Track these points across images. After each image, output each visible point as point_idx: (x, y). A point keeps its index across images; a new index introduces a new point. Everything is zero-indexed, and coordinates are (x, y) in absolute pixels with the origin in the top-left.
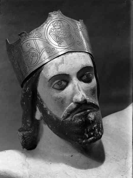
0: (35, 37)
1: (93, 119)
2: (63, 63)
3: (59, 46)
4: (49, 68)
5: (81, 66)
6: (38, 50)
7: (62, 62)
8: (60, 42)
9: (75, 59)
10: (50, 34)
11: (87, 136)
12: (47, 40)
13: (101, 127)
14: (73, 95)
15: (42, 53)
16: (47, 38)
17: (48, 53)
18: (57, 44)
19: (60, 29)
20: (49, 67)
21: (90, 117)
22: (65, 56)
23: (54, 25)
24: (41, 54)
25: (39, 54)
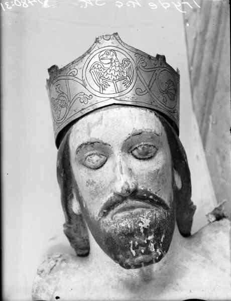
1: (147, 226)
2: (101, 124)
3: (101, 92)
6: (69, 96)
7: (100, 121)
8: (103, 87)
10: (91, 71)
11: (134, 252)
13: (162, 241)
14: (113, 182)
18: (98, 89)
23: (101, 57)
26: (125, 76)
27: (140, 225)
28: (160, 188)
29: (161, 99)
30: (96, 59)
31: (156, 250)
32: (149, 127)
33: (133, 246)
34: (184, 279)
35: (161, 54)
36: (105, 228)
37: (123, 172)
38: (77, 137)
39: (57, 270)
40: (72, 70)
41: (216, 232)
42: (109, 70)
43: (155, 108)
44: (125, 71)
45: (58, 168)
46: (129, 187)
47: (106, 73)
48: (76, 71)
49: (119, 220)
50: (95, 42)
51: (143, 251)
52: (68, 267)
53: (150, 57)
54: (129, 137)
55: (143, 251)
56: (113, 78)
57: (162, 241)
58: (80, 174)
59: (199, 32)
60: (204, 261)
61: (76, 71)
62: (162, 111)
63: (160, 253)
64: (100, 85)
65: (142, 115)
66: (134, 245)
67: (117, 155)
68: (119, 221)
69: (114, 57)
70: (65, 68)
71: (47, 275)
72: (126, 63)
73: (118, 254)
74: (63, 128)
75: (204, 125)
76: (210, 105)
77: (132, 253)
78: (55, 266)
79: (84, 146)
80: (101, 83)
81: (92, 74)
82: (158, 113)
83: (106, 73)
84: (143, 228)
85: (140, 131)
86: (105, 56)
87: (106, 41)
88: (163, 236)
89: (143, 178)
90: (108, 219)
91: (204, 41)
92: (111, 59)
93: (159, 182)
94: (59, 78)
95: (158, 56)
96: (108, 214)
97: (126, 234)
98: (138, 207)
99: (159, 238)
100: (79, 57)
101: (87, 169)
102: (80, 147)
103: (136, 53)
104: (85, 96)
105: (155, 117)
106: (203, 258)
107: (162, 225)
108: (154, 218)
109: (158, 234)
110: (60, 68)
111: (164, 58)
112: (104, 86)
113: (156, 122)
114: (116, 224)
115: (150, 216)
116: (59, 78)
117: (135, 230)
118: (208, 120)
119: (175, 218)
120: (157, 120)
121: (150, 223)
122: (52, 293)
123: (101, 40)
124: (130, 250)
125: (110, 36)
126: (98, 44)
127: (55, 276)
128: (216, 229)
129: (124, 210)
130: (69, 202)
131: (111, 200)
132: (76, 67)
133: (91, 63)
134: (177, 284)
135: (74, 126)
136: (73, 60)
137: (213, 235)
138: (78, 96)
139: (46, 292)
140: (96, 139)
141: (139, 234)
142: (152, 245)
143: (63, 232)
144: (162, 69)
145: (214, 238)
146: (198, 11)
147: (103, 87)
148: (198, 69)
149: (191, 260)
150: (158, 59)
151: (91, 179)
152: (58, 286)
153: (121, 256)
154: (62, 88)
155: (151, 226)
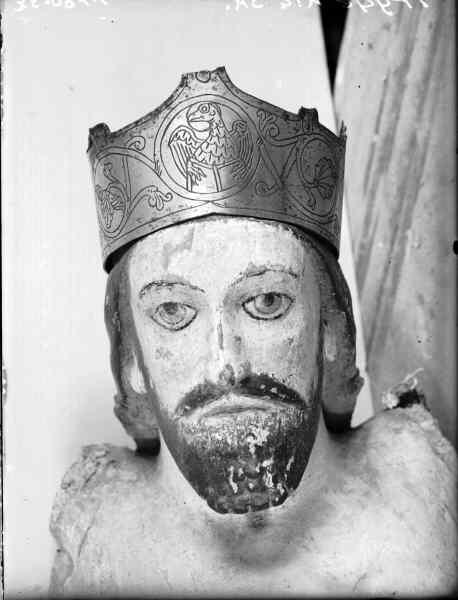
2: (189, 248)
3: (190, 189)
6: (128, 189)
8: (193, 177)
12: (156, 163)
13: (288, 468)
19: (207, 133)
21: (253, 435)
22: (202, 223)
27: (250, 439)
28: (293, 371)
29: (304, 202)
30: (181, 121)
31: (275, 486)
32: (280, 262)
33: (234, 477)
34: (325, 529)
35: (309, 106)
36: (186, 436)
37: (224, 345)
38: (142, 268)
39: (98, 483)
40: (134, 140)
41: (397, 431)
43: (292, 221)
45: (106, 307)
46: (233, 373)
47: (199, 151)
48: (142, 140)
49: (211, 427)
50: (181, 86)
51: (251, 486)
52: (116, 478)
53: (286, 115)
54: (241, 280)
55: (251, 486)
56: (212, 160)
57: (288, 468)
58: (148, 334)
59: (393, 70)
60: (367, 494)
61: (142, 140)
62: (306, 224)
63: (282, 491)
64: (187, 173)
65: (268, 236)
66: (236, 474)
67: (214, 298)
68: (212, 427)
69: (217, 118)
70: (122, 133)
71: (79, 493)
73: (207, 485)
74: (116, 248)
75: (396, 248)
76: (410, 209)
77: (231, 487)
78: (94, 473)
79: (154, 287)
82: (301, 231)
83: (199, 151)
84: (256, 445)
85: (263, 269)
86: (198, 114)
87: (203, 84)
88: (291, 460)
89: (261, 354)
90: (193, 420)
91: (401, 87)
92: (210, 122)
93: (291, 362)
94: (110, 151)
95: (303, 111)
96: (190, 414)
97: (223, 453)
98: (249, 408)
99: (284, 462)
100: (148, 112)
101: (158, 328)
102: (148, 287)
103: (260, 109)
104: (159, 194)
105: (294, 238)
106: (365, 486)
107: (291, 439)
108: (277, 426)
109: (281, 456)
110: (112, 131)
111: (314, 113)
112: (196, 177)
113: (294, 248)
114: (205, 433)
115: (269, 424)
116: (110, 151)
117: (239, 447)
118: (404, 238)
119: (317, 425)
120: (297, 243)
121: (267, 437)
122: (85, 529)
123: (193, 83)
124: (228, 482)
125: (210, 73)
126: (186, 90)
127: (94, 495)
128: (398, 426)
129: (223, 411)
130: (125, 369)
131: (200, 391)
132: (144, 133)
133: (172, 127)
134: (312, 539)
135: (139, 244)
136: (138, 118)
137: (390, 436)
138: (144, 193)
139: (75, 524)
140: (178, 277)
141: (248, 455)
142: (270, 475)
144: (312, 137)
145: (389, 444)
146: (393, 28)
147: (192, 179)
148: (389, 140)
149: (341, 490)
150: (302, 118)
151: (165, 346)
152: (98, 516)
153: (211, 490)
154: (115, 172)
155: (270, 441)
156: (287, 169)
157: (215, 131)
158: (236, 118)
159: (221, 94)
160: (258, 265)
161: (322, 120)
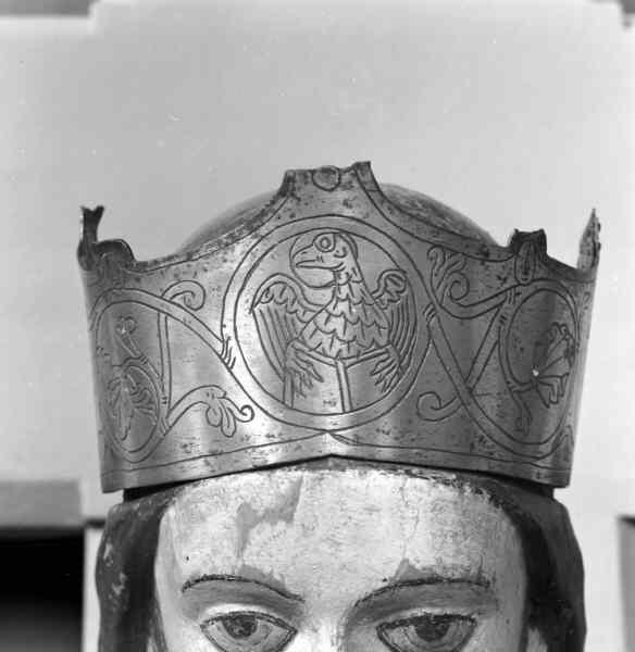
0: (169, 295)
2: (289, 519)
3: (288, 403)
4: (203, 518)
5: (395, 566)
7: (284, 511)
9: (371, 510)
12: (225, 343)
15: (181, 408)
16: (232, 335)
17: (209, 422)
19: (328, 292)
20: (202, 507)
22: (316, 474)
23: (296, 261)
24: (494, 301)
25: (164, 408)
26: (383, 342)
35: (528, 227)
40: (184, 286)
42: (324, 315)
44: (384, 323)
47: (312, 326)
69: (348, 262)
72: (391, 287)
80: (291, 364)
81: (259, 318)
83: (312, 326)
86: (312, 253)
92: (336, 271)
95: (519, 238)
111: (539, 239)
123: (305, 190)
135: (187, 488)
143: (283, 176)
144: (531, 289)
156: (479, 366)
157: (345, 290)
158: (387, 264)
159: (360, 217)
160: (418, 566)
161: (553, 252)
